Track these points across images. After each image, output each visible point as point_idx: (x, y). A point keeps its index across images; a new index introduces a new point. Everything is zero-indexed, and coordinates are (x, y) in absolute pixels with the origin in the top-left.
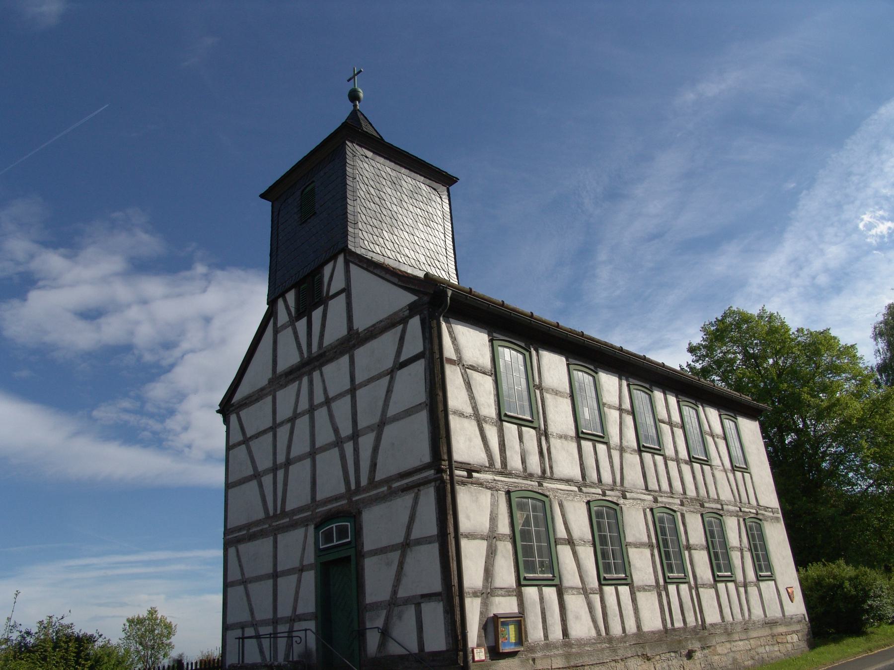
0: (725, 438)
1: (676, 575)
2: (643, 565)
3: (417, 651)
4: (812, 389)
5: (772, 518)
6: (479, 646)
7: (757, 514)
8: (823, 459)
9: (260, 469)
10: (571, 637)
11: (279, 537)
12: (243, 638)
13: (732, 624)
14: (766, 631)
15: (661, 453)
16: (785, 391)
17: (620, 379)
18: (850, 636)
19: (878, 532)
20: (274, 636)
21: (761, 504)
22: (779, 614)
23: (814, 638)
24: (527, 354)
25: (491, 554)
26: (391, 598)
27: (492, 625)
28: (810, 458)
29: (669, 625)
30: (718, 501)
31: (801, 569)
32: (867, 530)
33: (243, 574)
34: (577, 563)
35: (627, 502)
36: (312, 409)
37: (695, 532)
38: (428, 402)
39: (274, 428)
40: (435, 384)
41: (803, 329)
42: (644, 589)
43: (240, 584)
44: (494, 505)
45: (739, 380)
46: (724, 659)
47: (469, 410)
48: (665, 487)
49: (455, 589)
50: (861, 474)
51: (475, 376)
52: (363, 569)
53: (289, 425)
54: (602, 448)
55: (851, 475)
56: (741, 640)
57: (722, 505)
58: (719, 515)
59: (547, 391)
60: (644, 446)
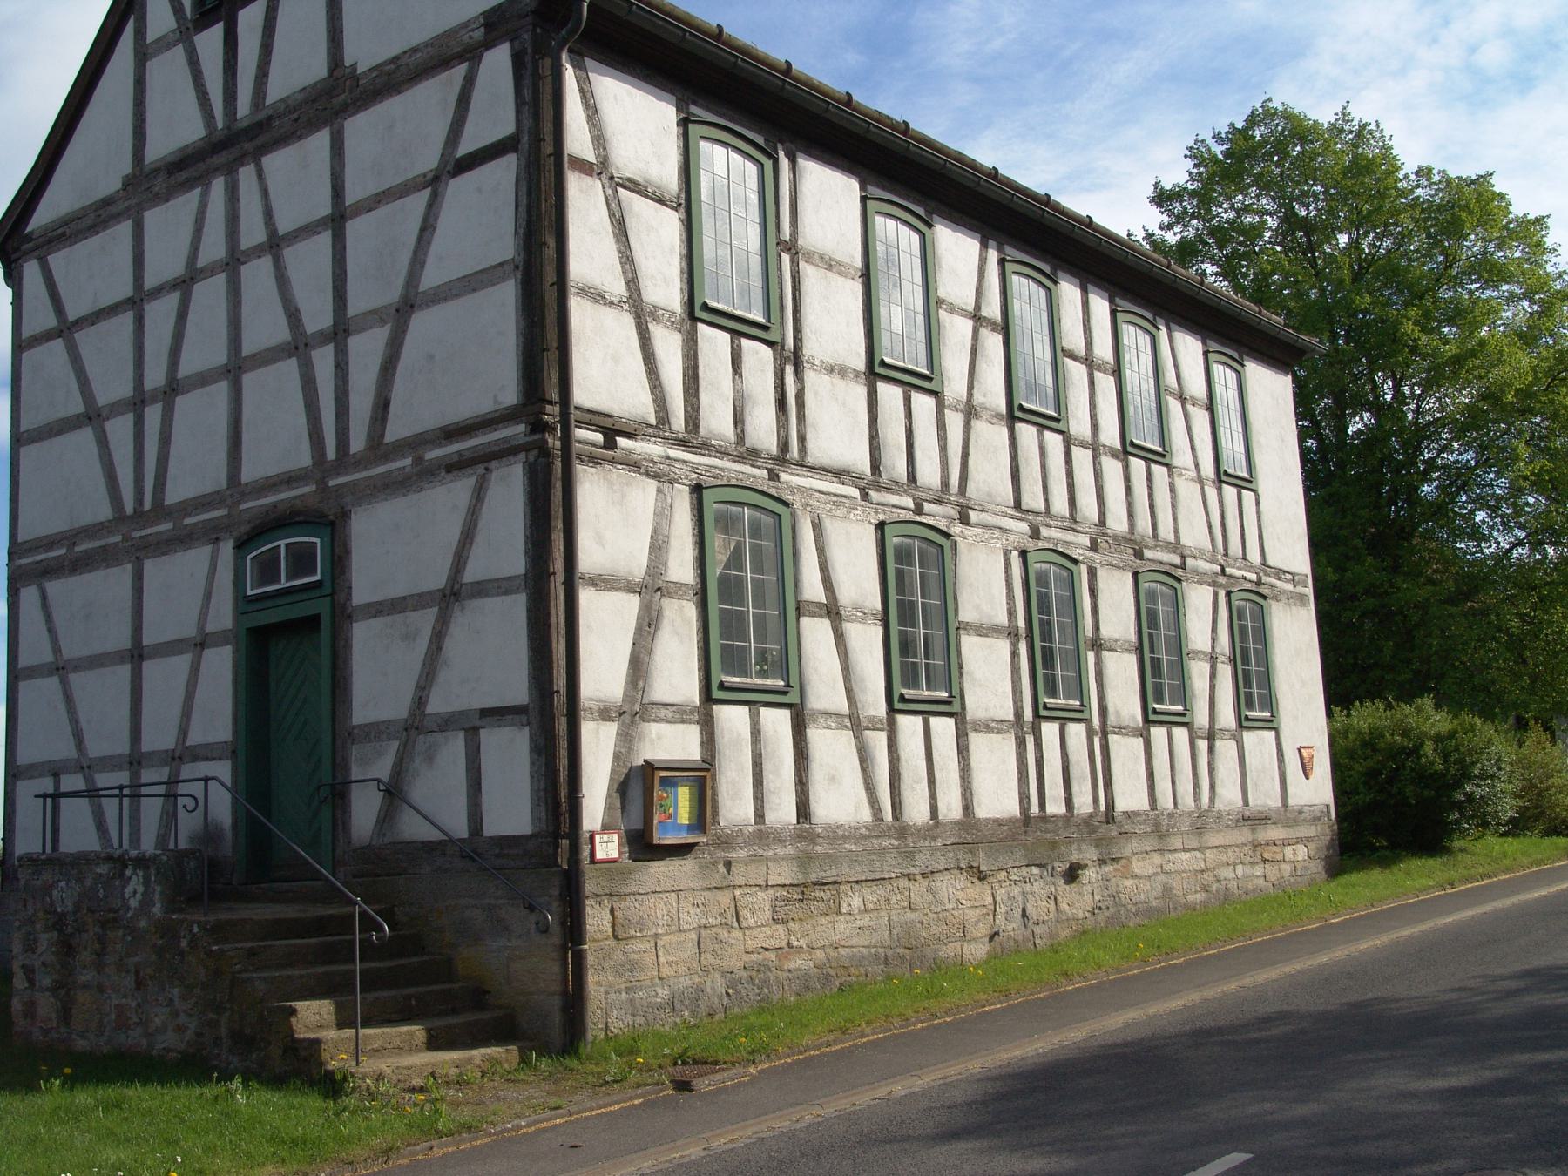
0: (1211, 407)
1: (1061, 701)
2: (990, 674)
3: (465, 836)
4: (1427, 315)
5: (1290, 596)
6: (606, 828)
7: (1259, 583)
8: (1425, 477)
9: (102, 400)
10: (815, 820)
11: (149, 565)
12: (56, 796)
13: (1170, 815)
14: (1243, 835)
15: (1060, 426)
16: (1365, 312)
17: (984, 245)
18: (1414, 855)
19: (1516, 646)
20: (134, 792)
21: (1271, 562)
22: (1274, 802)
23: (1341, 854)
24: (768, 164)
25: (648, 625)
26: (412, 714)
27: (640, 784)
28: (1397, 471)
29: (1035, 809)
30: (1176, 547)
31: (1337, 710)
32: (1494, 638)
33: (57, 650)
34: (842, 661)
35: (968, 531)
36: (234, 262)
37: (1115, 608)
38: (520, 260)
39: (136, 303)
40: (539, 217)
41: (1430, 169)
42: (988, 726)
43: (50, 674)
44: (663, 516)
45: (1262, 279)
46: (1145, 886)
47: (618, 289)
48: (1060, 505)
49: (560, 700)
50: (1503, 516)
51: (639, 209)
52: (348, 645)
53: (174, 298)
54: (923, 404)
55: (1480, 516)
56: (1185, 850)
57: (1183, 557)
58: (1172, 577)
59: (809, 257)
60: (1021, 408)
